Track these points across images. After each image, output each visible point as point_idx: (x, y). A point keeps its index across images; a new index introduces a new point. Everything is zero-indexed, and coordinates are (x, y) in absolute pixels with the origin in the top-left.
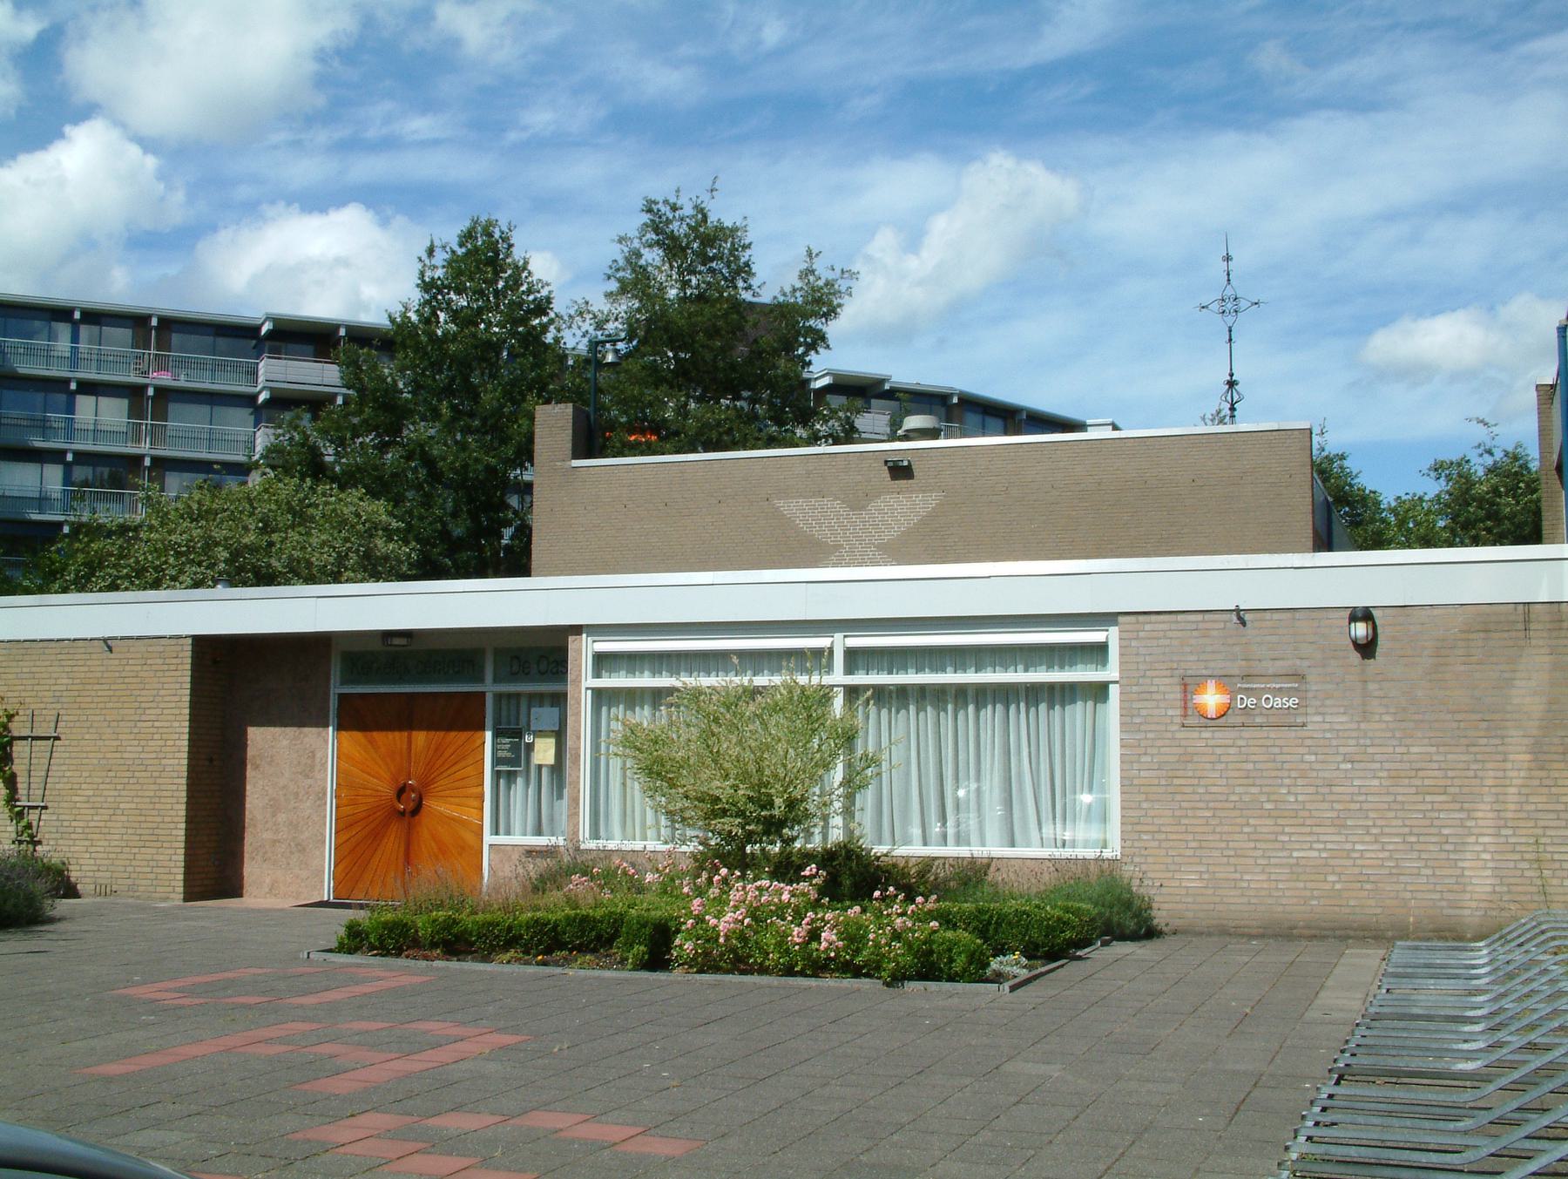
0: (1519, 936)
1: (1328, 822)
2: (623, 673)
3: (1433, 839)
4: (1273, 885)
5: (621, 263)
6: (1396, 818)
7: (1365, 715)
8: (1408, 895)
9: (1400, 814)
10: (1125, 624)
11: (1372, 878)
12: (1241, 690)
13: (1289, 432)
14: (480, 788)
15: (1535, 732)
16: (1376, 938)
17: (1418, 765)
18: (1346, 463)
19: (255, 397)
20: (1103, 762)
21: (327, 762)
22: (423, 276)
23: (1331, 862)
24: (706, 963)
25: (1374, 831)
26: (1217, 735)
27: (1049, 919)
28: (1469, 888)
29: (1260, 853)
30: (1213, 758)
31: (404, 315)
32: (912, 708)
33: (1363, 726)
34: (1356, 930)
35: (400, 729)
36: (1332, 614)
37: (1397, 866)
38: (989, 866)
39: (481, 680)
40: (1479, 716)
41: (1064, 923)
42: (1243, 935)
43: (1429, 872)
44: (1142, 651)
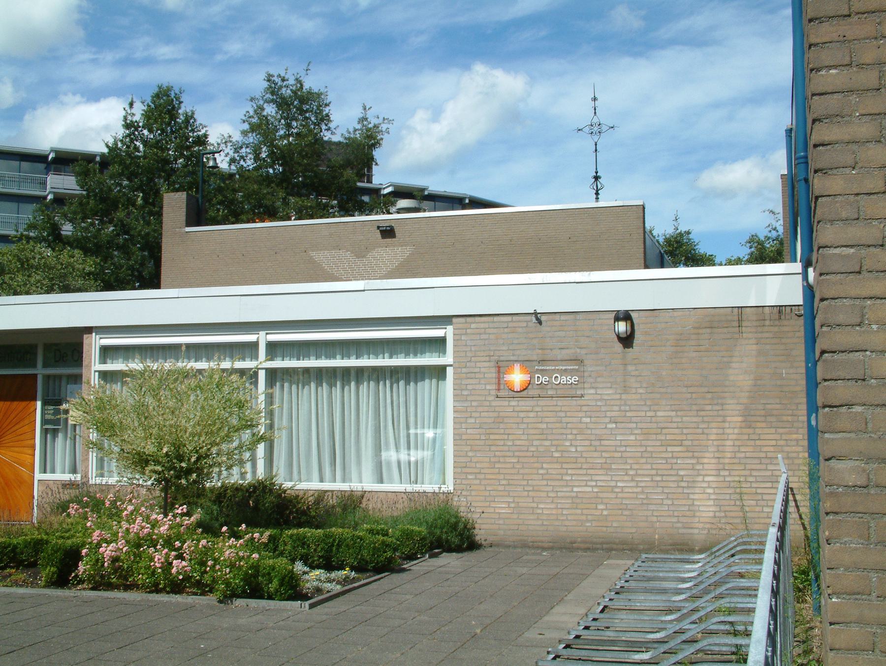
0: (731, 549)
1: (599, 466)
2: (120, 360)
3: (674, 478)
4: (560, 511)
5: (252, 113)
6: (646, 463)
7: (626, 389)
8: (655, 519)
9: (649, 460)
10: (457, 323)
11: (629, 507)
12: (538, 371)
13: (630, 207)
14: (33, 441)
15: (745, 401)
16: (631, 550)
17: (662, 425)
18: (691, 236)
19: (45, 198)
20: (443, 421)
22: (126, 120)
23: (600, 495)
24: (100, 583)
25: (631, 472)
26: (521, 403)
27: (376, 543)
28: (698, 514)
29: (550, 488)
30: (518, 420)
31: (116, 143)
32: (313, 385)
33: (624, 397)
34: (617, 544)
36: (602, 316)
37: (647, 498)
38: (362, 497)
39: (34, 366)
40: (706, 389)
41: (387, 546)
42: (538, 547)
43: (670, 502)
44: (469, 343)
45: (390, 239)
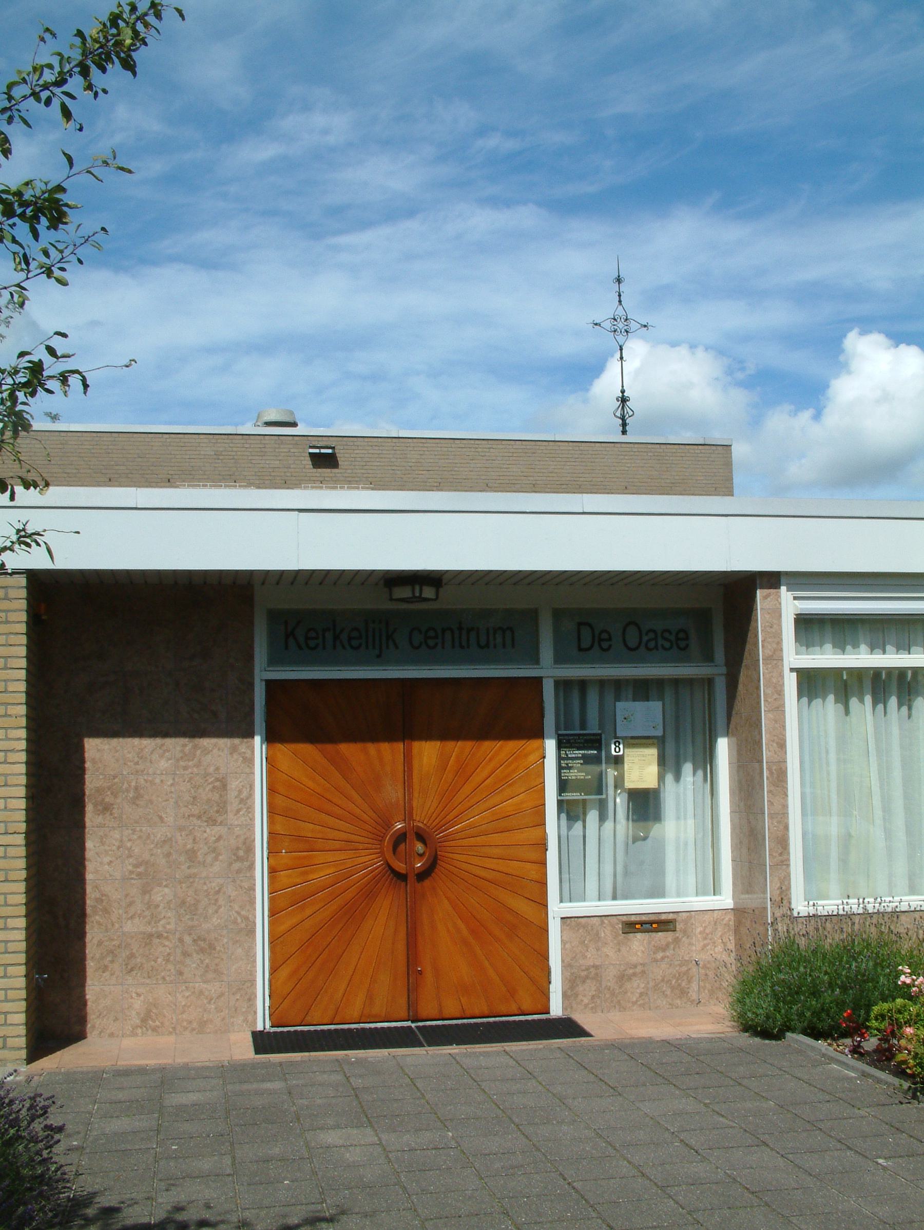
13: (714, 448)
21: (251, 795)
35: (391, 737)
45: (329, 470)
